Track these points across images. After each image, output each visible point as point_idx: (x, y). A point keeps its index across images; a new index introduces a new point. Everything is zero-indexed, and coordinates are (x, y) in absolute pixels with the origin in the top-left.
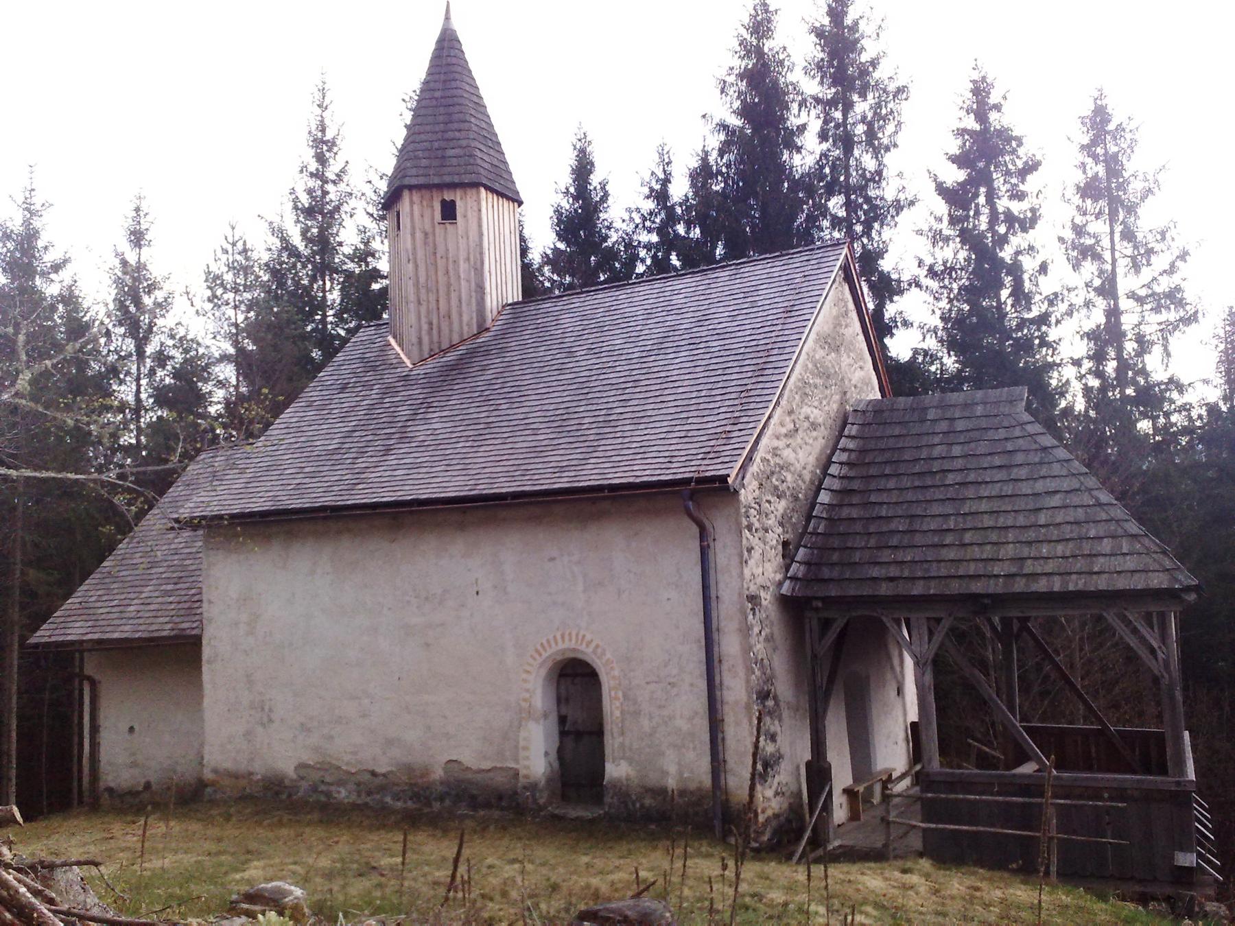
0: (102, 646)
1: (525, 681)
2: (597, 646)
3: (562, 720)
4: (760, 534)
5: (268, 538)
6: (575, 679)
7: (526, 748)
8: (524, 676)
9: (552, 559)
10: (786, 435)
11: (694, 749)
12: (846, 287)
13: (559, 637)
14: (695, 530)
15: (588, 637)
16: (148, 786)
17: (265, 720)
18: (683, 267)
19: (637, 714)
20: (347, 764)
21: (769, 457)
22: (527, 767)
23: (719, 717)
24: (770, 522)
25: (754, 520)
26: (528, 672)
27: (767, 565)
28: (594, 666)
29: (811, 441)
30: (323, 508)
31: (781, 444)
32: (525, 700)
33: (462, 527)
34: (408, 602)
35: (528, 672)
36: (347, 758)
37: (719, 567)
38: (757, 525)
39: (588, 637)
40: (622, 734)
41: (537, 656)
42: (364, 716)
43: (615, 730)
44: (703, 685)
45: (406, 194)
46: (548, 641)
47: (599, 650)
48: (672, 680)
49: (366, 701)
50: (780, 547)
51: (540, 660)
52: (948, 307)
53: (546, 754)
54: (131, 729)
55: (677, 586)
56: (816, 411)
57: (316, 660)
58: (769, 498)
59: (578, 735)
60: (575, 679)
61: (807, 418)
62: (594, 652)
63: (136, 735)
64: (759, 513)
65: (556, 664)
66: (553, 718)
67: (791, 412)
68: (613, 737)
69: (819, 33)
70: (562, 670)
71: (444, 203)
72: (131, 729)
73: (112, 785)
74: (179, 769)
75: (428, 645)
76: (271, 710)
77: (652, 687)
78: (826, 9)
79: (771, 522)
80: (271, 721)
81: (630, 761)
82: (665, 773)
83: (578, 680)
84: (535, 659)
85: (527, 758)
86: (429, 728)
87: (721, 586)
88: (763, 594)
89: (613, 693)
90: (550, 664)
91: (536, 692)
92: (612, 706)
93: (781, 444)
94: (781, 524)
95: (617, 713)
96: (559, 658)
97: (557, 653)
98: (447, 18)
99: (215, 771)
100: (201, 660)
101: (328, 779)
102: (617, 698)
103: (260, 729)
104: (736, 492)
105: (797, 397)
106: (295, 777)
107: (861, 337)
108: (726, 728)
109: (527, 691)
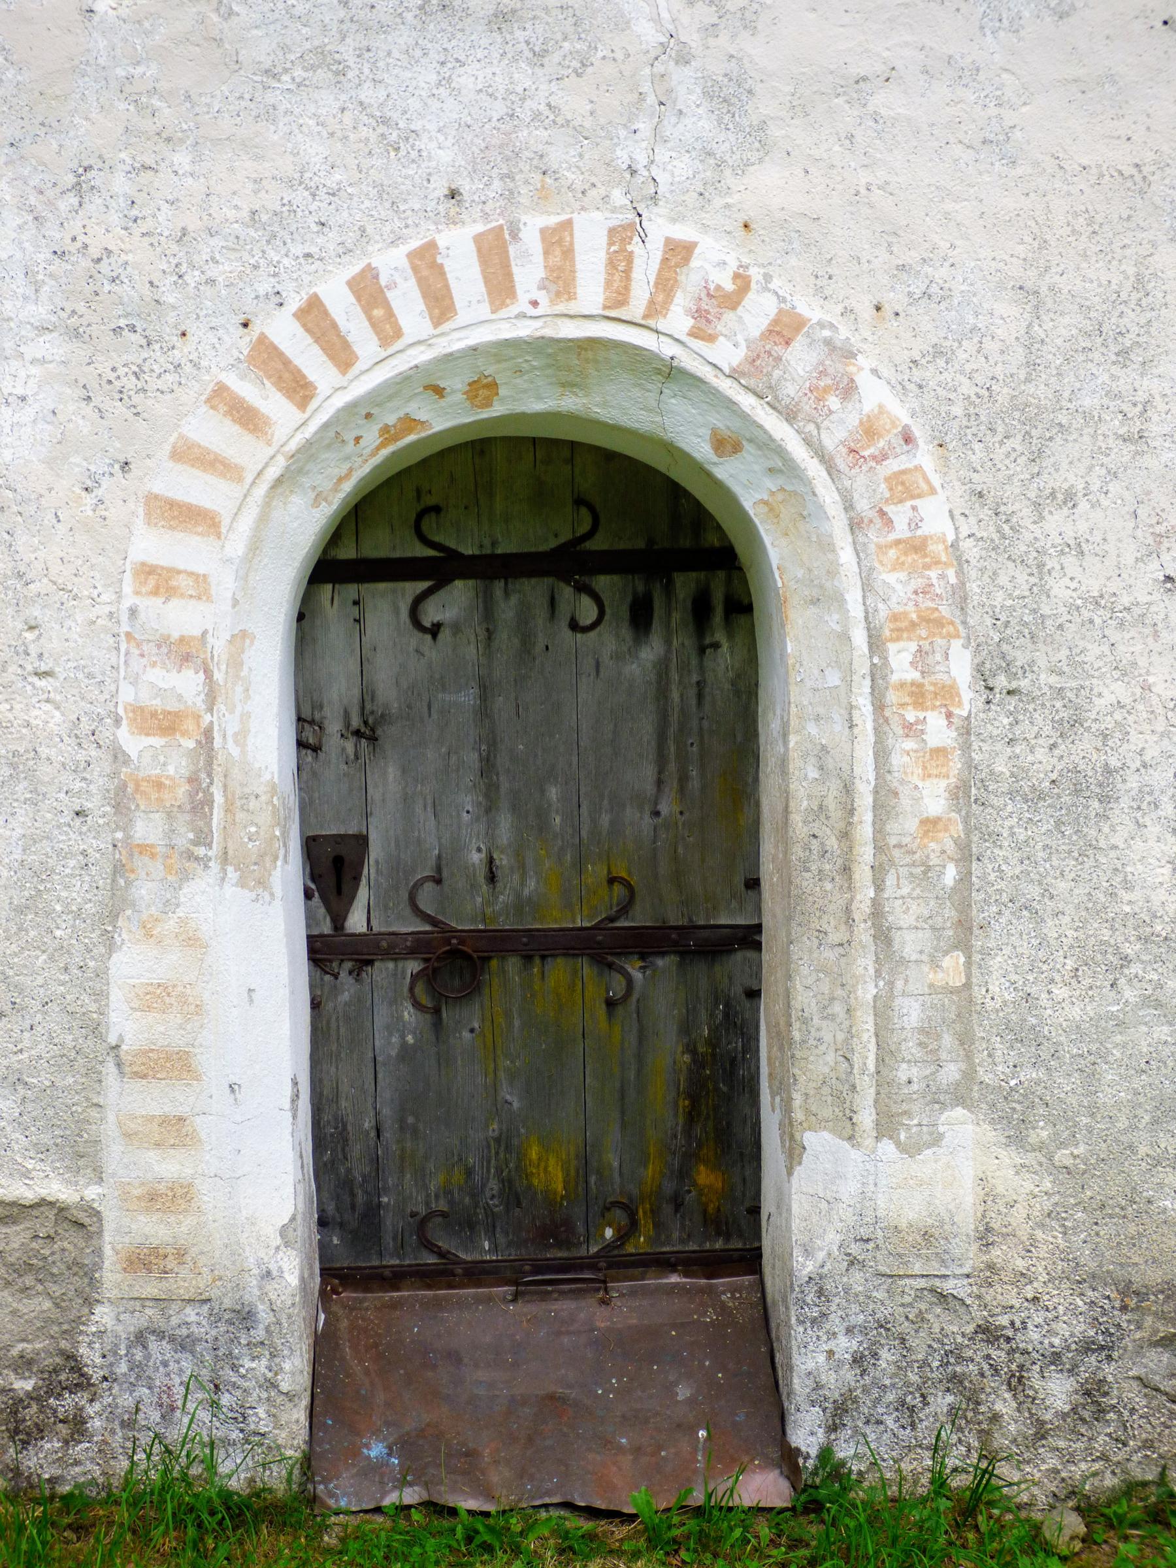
1: (159, 580)
2: (785, 328)
3: (331, 868)
7: (174, 1064)
8: (152, 545)
13: (247, 390)
15: (715, 261)
32: (165, 723)
39: (715, 261)
40: (965, 934)
41: (273, 404)
43: (909, 913)
46: (369, 291)
62: (757, 370)
81: (1014, 1114)
83: (454, 603)
84: (247, 418)
85: (175, 1131)
89: (901, 661)
95: (934, 799)
109: (184, 652)
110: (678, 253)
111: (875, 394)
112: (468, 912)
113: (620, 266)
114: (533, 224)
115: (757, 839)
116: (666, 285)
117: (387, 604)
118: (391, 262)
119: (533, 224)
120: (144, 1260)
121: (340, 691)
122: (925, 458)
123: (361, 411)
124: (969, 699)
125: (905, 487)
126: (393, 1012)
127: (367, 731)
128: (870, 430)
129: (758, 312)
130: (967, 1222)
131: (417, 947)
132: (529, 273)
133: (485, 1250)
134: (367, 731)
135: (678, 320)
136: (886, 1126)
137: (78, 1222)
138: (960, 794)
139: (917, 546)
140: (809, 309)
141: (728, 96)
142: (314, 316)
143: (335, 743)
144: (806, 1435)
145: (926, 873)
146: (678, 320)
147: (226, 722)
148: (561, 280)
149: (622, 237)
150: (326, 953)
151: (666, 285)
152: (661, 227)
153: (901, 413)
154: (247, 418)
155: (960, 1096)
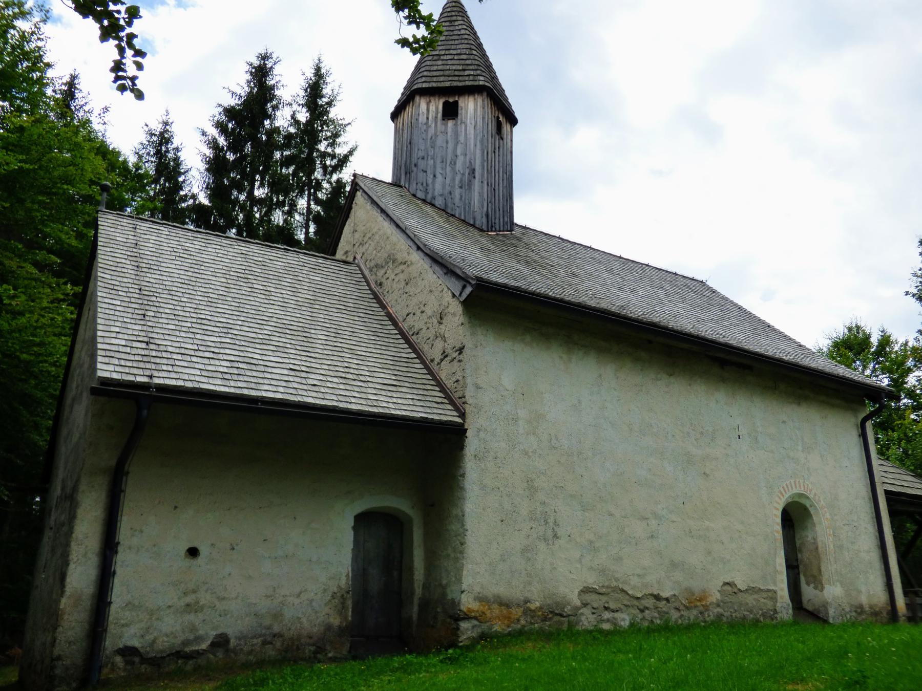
9: (784, 422)
16: (221, 642)
17: (550, 533)
36: (635, 581)
49: (654, 522)
52: (415, 275)
54: (193, 552)
60: (794, 518)
63: (200, 560)
69: (403, 47)
72: (193, 552)
74: (289, 614)
80: (556, 536)
82: (860, 592)
99: (481, 599)
101: (612, 606)
103: (542, 546)
106: (578, 603)
118: (792, 481)
137: (775, 592)
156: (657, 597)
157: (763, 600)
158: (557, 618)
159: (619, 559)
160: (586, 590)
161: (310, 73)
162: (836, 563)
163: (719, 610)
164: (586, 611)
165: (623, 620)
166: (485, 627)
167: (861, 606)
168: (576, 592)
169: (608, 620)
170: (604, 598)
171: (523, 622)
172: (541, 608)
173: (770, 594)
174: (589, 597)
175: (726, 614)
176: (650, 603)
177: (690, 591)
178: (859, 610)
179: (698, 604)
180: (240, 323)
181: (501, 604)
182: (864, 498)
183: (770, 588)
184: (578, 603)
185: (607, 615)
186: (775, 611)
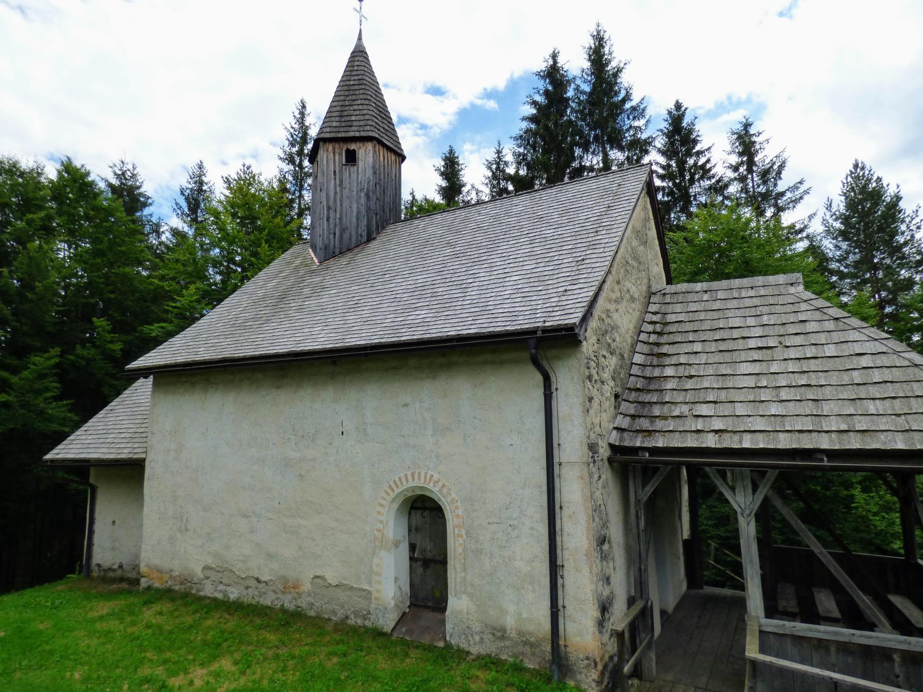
0: (102, 464)
1: (379, 513)
2: (444, 486)
3: (412, 547)
4: (599, 385)
5: (193, 384)
6: (424, 513)
7: (379, 574)
8: (378, 508)
9: (406, 405)
10: (615, 301)
11: (534, 591)
12: (648, 200)
13: (388, 490)
14: (539, 378)
15: (436, 477)
18: (516, 190)
19: (478, 552)
20: (239, 570)
21: (604, 316)
22: (378, 591)
23: (559, 563)
24: (605, 375)
25: (594, 372)
26: (382, 505)
27: (604, 415)
28: (440, 503)
29: (631, 311)
30: (224, 360)
31: (612, 307)
32: (379, 531)
33: (333, 376)
34: (289, 439)
35: (382, 505)
37: (561, 415)
38: (596, 377)
39: (436, 477)
40: (465, 570)
41: (391, 493)
42: (252, 532)
43: (458, 566)
44: (544, 530)
45: (321, 144)
46: (400, 479)
47: (445, 490)
48: (512, 523)
49: (255, 519)
50: (613, 399)
51: (392, 495)
53: (396, 579)
55: (519, 433)
56: (634, 288)
57: (212, 486)
58: (605, 353)
59: (426, 563)
60: (424, 513)
61: (628, 291)
62: (440, 491)
64: (598, 365)
65: (407, 500)
66: (404, 548)
67: (618, 282)
68: (456, 572)
70: (413, 503)
71: (348, 151)
73: (100, 562)
75: (301, 476)
76: (187, 521)
77: (494, 527)
78: (553, 191)
79: (606, 375)
80: (187, 530)
81: (471, 596)
82: (504, 612)
83: (426, 514)
84: (388, 494)
85: (379, 583)
86: (300, 547)
87: (563, 433)
88: (600, 443)
89: (457, 532)
90: (402, 498)
91: (391, 526)
92: (455, 544)
93: (612, 307)
94: (614, 379)
95: (460, 550)
96: (410, 494)
97: (407, 490)
98: (360, 38)
99: (148, 566)
100: (143, 478)
102: (460, 536)
103: (179, 535)
104: (580, 342)
105: (622, 271)
106: (202, 576)
107: (657, 242)
108: (566, 574)
109: (381, 522)
110: (432, 476)
111: (453, 495)
112: (429, 555)
113: (425, 477)
114: (417, 472)
115: (31, 585)
116: (430, 480)
117: (419, 513)
118: (409, 474)
119: (417, 472)
120: (376, 599)
121: (414, 524)
122: (459, 504)
123: (401, 493)
124: (465, 537)
125: (457, 508)
126: (420, 570)
127: (417, 529)
128: (453, 500)
129: (441, 483)
130: (465, 611)
131: (422, 560)
132: (416, 478)
133: (430, 604)
134: (417, 529)
135: (432, 484)
136: (455, 596)
137: (369, 592)
138: (464, 550)
139: (458, 516)
140: (446, 483)
141: (437, 457)
142: (413, 474)
143: (414, 531)
144: (448, 639)
145: (460, 561)
146: (432, 484)
147: (385, 531)
148: (419, 479)
149: (426, 473)
150: (412, 559)
151: (430, 480)
152: (430, 473)
153: (456, 498)
154: (388, 494)
155: (464, 593)
156: (258, 581)
157: (356, 598)
158: (188, 584)
159: (228, 547)
160: (206, 568)
161: (590, 42)
162: (465, 570)
163: (310, 599)
164: (208, 582)
165: (232, 593)
166: (150, 583)
167: (503, 630)
168: (200, 568)
169: (221, 591)
170: (220, 575)
171: (170, 583)
172: (179, 576)
173: (364, 593)
174: (209, 573)
175: (316, 604)
176: (253, 583)
177: (285, 580)
178: (499, 634)
179: (293, 590)
180: (460, 303)
181: (158, 571)
182: (540, 487)
183: (365, 588)
184: (202, 576)
185: (221, 587)
186: (369, 613)
